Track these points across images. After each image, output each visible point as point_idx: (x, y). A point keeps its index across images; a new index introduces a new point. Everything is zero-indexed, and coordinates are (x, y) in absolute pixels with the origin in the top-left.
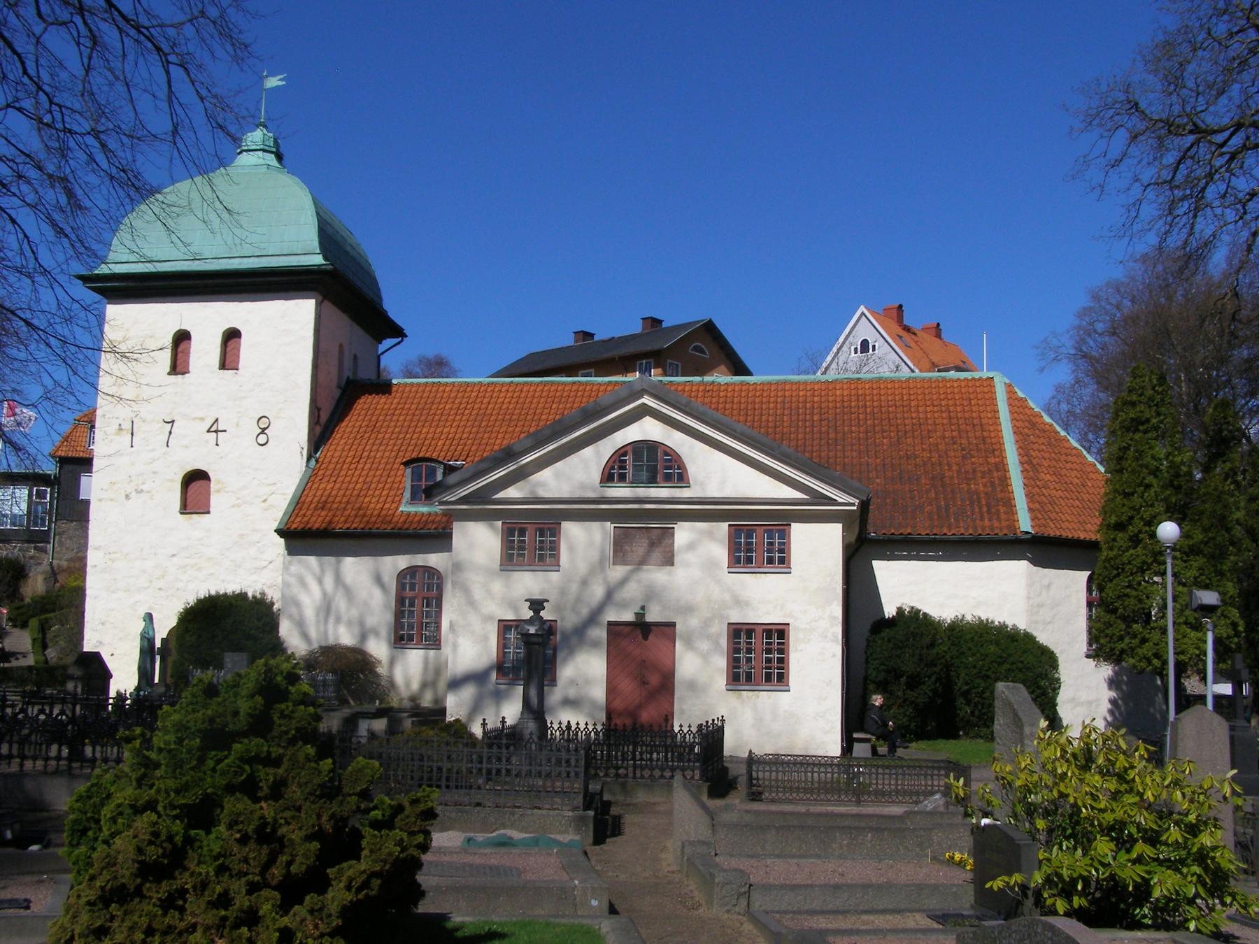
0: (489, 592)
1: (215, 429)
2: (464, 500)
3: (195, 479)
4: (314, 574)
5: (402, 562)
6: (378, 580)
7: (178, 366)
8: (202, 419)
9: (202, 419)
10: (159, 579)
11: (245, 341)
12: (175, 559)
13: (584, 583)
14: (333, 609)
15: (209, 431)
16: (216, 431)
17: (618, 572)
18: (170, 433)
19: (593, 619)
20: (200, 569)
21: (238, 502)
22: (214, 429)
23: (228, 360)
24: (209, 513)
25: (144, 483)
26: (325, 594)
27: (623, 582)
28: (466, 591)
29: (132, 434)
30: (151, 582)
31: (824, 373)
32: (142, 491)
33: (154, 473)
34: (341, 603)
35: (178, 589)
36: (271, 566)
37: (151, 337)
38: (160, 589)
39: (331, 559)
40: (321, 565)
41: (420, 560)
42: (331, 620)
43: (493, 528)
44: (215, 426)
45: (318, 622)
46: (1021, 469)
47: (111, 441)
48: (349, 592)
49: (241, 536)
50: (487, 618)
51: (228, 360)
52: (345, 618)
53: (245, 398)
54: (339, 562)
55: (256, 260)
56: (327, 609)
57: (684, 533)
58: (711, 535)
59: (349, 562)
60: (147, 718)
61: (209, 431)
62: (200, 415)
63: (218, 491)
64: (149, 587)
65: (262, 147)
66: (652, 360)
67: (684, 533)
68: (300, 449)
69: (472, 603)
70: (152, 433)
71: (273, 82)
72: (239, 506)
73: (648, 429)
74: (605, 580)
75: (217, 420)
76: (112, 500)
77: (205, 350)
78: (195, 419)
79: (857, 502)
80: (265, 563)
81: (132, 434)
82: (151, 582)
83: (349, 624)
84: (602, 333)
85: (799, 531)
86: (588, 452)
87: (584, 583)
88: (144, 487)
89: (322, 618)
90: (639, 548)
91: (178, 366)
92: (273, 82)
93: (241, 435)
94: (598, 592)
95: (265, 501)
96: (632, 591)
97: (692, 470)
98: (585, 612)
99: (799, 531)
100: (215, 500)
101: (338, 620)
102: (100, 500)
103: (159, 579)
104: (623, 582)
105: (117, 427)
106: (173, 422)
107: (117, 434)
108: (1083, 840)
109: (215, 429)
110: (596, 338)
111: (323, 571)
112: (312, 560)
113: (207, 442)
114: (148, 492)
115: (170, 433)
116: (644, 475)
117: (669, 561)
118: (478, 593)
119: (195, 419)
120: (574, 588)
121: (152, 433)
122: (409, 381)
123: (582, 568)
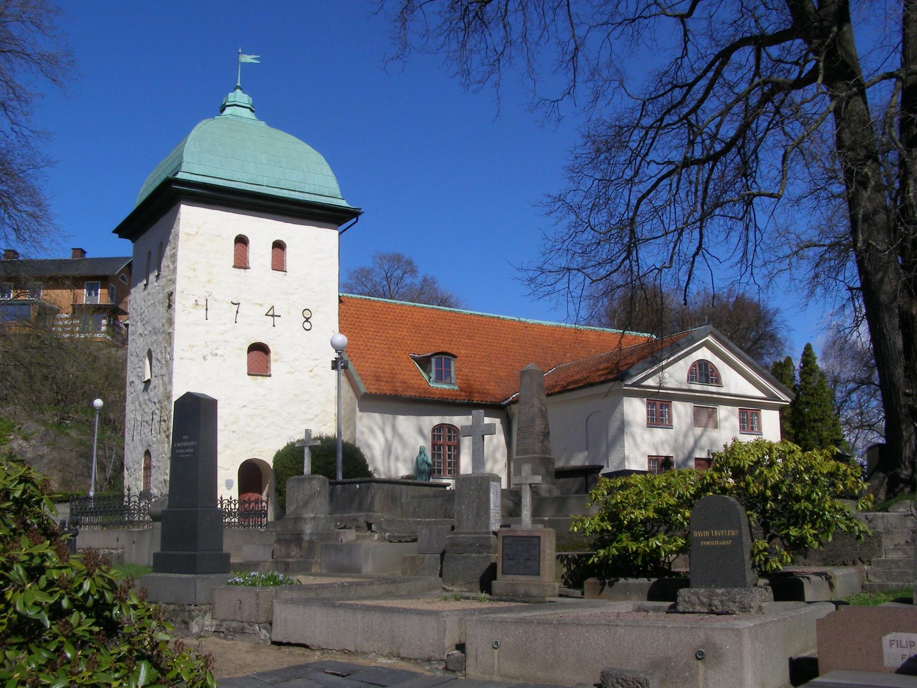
0: (643, 439)
1: (272, 314)
2: (633, 385)
3: (259, 349)
4: (379, 427)
5: (436, 420)
6: (421, 432)
7: (241, 263)
8: (261, 305)
9: (261, 305)
10: (232, 424)
11: (288, 250)
12: (244, 409)
13: (686, 436)
14: (393, 450)
15: (266, 315)
16: (273, 316)
17: (698, 431)
18: (237, 312)
19: (689, 456)
20: (263, 418)
21: (292, 370)
22: (272, 314)
23: (279, 265)
24: (270, 376)
25: (217, 349)
26: (387, 441)
27: (702, 435)
28: (634, 437)
29: (207, 310)
32: (216, 355)
33: (226, 341)
34: (397, 446)
35: (248, 432)
36: (316, 419)
37: (219, 236)
38: (234, 432)
39: (390, 416)
40: (383, 419)
41: (447, 420)
42: (392, 458)
43: (643, 401)
44: (272, 311)
45: (383, 459)
47: (189, 313)
48: (400, 437)
49: (295, 395)
50: (643, 454)
51: (279, 265)
52: (401, 458)
54: (394, 419)
55: (300, 194)
56: (388, 450)
57: (723, 411)
58: (732, 412)
59: (401, 419)
61: (266, 315)
62: (260, 302)
63: (276, 361)
65: (249, 106)
66: (99, 282)
67: (723, 411)
69: (636, 445)
70: (222, 312)
71: (247, 59)
72: (292, 373)
73: (704, 354)
74: (694, 436)
76: (192, 359)
77: (261, 253)
78: (255, 304)
79: (790, 400)
80: (312, 417)
81: (207, 310)
83: (405, 461)
84: (92, 253)
85: (765, 413)
86: (681, 362)
87: (686, 436)
88: (218, 352)
89: (386, 454)
90: (704, 418)
91: (241, 263)
92: (247, 59)
93: (292, 321)
94: (691, 441)
95: (311, 371)
96: (704, 441)
98: (686, 452)
99: (765, 413)
100: (274, 367)
101: (397, 459)
102: (182, 359)
103: (232, 424)
104: (702, 435)
105: (194, 302)
107: (194, 308)
110: (87, 256)
111: (384, 424)
112: (377, 416)
113: (266, 322)
114: (222, 356)
115: (237, 312)
116: (704, 378)
117: (716, 426)
118: (638, 439)
119: (255, 304)
120: (681, 439)
121: (222, 312)
122: (350, 295)
123: (684, 427)
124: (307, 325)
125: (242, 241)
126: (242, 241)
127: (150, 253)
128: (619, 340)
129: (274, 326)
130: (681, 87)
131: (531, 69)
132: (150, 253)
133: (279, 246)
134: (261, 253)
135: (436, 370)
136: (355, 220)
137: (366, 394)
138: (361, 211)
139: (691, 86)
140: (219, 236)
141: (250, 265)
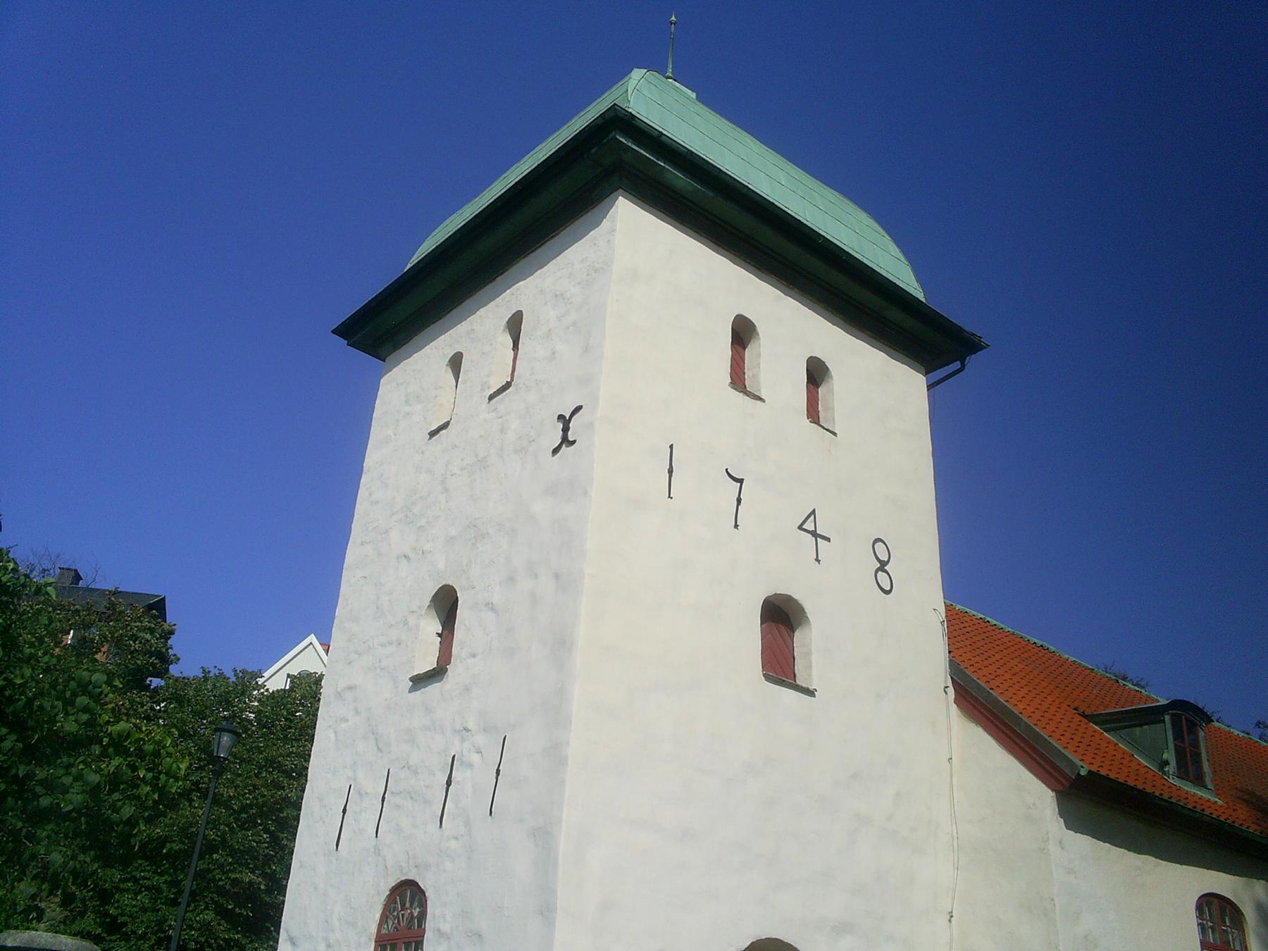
15: (800, 527)
16: (814, 534)
61: (800, 527)
81: (671, 471)
126: (742, 333)
133: (816, 373)
135: (1176, 745)
136: (957, 365)
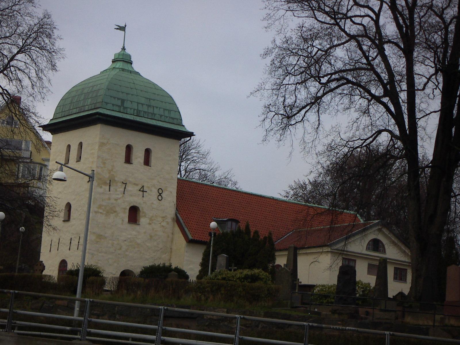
1: (142, 190)
7: (128, 160)
12: (125, 242)
15: (139, 190)
16: (143, 191)
23: (147, 162)
30: (115, 250)
31: (213, 270)
37: (118, 145)
44: (142, 189)
46: (321, 285)
51: (147, 162)
53: (153, 179)
60: (360, 184)
61: (139, 190)
64: (114, 253)
68: (174, 205)
75: (143, 186)
77: (138, 156)
82: (115, 250)
91: (128, 160)
97: (387, 251)
106: (126, 183)
108: (209, 284)
109: (142, 190)
113: (139, 195)
124: (160, 198)
125: (129, 149)
126: (129, 149)
127: (69, 146)
128: (298, 115)
129: (143, 197)
130: (362, 140)
131: (283, 49)
132: (69, 146)
133: (148, 152)
134: (138, 156)
137: (191, 240)
138: (194, 134)
139: (366, 140)
140: (118, 145)
141: (133, 162)
